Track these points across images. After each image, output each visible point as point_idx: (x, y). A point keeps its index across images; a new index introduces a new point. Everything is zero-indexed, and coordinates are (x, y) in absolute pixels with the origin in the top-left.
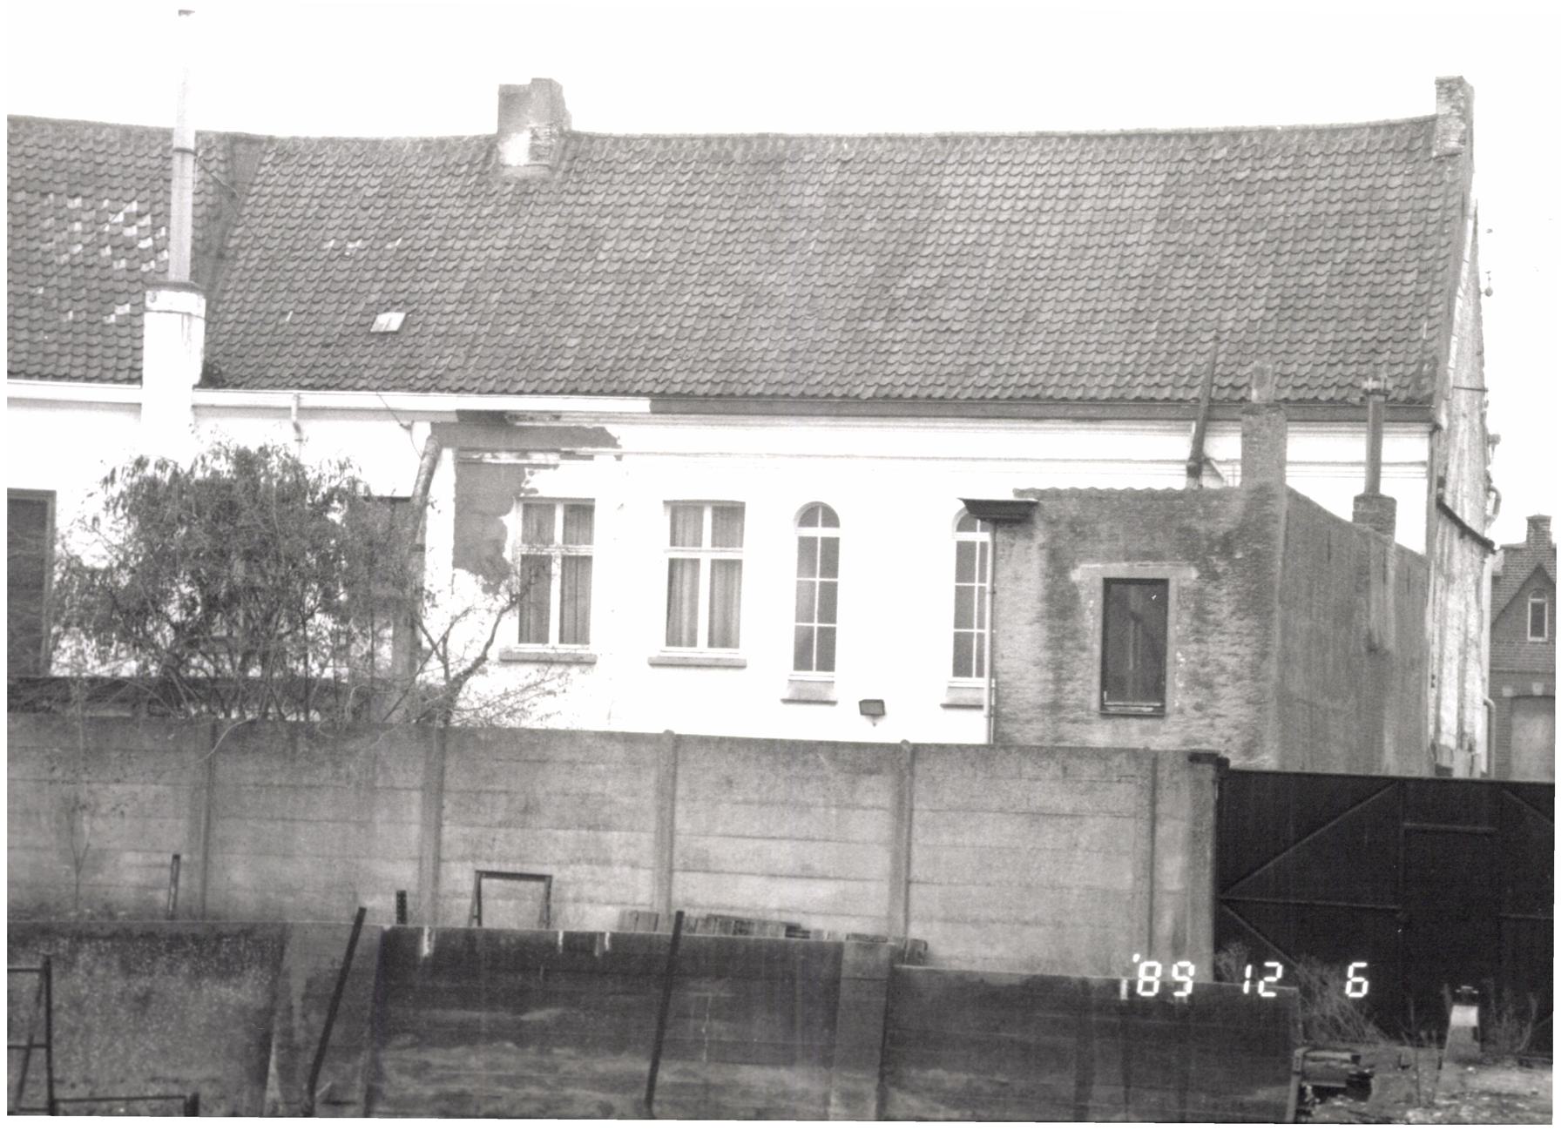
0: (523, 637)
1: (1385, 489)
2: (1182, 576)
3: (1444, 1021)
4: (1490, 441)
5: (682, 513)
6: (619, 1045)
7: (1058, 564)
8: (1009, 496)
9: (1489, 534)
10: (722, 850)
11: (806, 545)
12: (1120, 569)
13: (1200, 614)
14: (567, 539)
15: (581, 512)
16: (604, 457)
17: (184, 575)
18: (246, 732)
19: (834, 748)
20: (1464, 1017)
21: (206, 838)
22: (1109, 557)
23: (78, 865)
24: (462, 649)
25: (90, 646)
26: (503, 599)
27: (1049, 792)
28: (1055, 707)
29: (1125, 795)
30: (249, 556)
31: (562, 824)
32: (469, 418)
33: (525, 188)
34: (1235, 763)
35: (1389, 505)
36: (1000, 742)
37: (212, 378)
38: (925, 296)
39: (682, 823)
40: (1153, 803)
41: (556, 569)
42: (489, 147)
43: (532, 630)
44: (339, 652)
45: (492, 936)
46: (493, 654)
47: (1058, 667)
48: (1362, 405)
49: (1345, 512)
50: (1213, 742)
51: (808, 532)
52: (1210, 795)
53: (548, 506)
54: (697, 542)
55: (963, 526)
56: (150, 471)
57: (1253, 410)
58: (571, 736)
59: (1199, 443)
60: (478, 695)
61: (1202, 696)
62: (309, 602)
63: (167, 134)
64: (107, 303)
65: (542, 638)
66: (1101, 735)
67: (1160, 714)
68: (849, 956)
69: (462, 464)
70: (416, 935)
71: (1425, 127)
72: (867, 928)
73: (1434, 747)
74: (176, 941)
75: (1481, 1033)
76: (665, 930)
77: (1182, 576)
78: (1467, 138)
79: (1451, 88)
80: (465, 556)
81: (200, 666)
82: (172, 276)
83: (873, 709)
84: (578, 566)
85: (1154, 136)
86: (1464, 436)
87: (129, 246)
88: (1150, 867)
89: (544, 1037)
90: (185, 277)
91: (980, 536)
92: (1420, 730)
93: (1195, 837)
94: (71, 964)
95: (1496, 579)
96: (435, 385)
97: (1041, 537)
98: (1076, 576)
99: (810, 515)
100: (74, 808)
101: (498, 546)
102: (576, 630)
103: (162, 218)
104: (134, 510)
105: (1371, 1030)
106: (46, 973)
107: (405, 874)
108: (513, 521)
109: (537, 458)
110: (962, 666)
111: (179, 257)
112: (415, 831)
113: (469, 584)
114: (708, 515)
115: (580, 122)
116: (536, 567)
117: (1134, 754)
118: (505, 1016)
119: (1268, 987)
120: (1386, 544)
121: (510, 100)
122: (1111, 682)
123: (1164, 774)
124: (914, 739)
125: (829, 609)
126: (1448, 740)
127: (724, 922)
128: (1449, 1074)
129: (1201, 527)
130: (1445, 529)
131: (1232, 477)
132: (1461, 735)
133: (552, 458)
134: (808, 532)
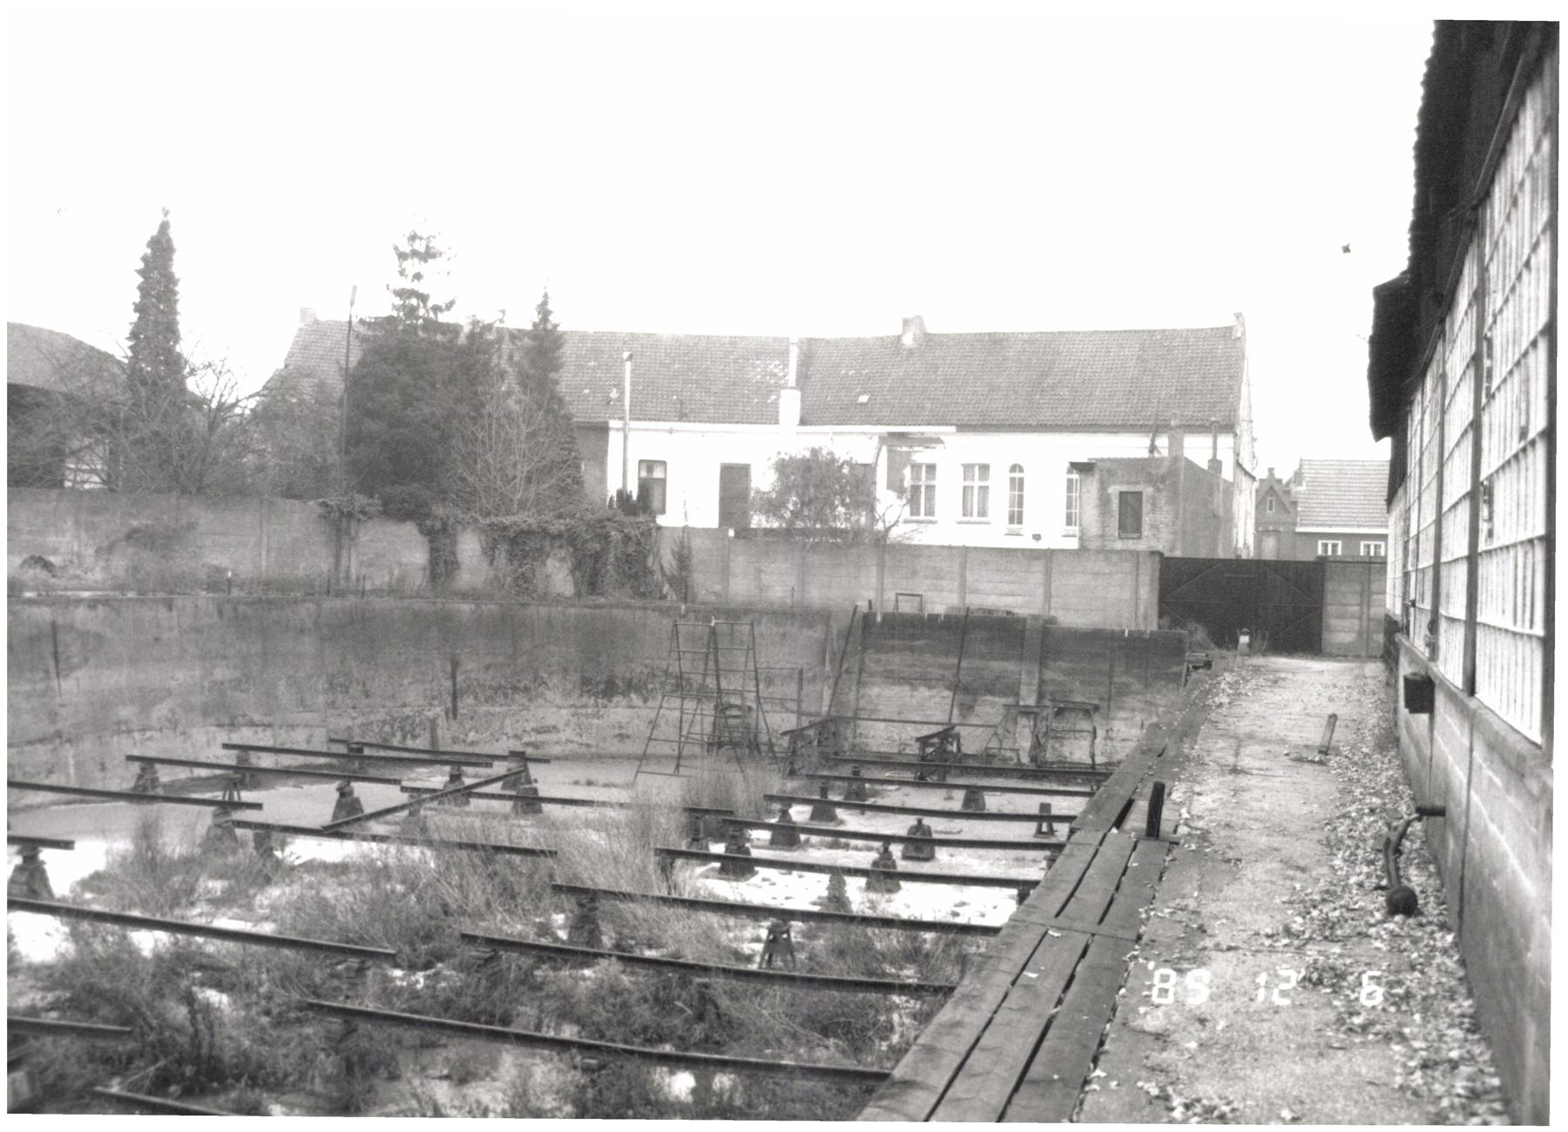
0: (912, 514)
1: (1218, 457)
2: (1148, 491)
3: (1237, 641)
4: (1254, 440)
5: (968, 468)
6: (947, 653)
7: (1103, 487)
8: (1086, 461)
9: (1254, 474)
10: (983, 586)
11: (1012, 480)
12: (1125, 488)
13: (1154, 504)
14: (927, 478)
15: (931, 468)
16: (939, 447)
17: (794, 493)
18: (814, 547)
19: (1023, 551)
20: (1244, 639)
21: (802, 582)
22: (1122, 483)
23: (761, 590)
24: (890, 520)
25: (763, 518)
26: (904, 501)
27: (1100, 565)
28: (1102, 536)
29: (1127, 566)
30: (816, 486)
31: (927, 577)
32: (891, 435)
33: (911, 352)
34: (1167, 554)
35: (1220, 463)
36: (1083, 548)
37: (803, 422)
38: (1054, 387)
39: (969, 578)
40: (1138, 569)
41: (923, 490)
42: (899, 338)
43: (915, 511)
44: (847, 520)
45: (901, 615)
46: (901, 520)
47: (1103, 522)
48: (1210, 427)
49: (1204, 465)
50: (1160, 547)
51: (1013, 475)
52: (1158, 566)
53: (920, 466)
54: (973, 479)
55: (1069, 472)
56: (782, 456)
57: (1172, 429)
58: (929, 547)
59: (1153, 441)
60: (895, 534)
61: (1154, 531)
62: (837, 502)
63: (788, 339)
64: (768, 396)
65: (918, 513)
66: (1119, 545)
67: (1140, 538)
68: (1029, 621)
69: (889, 451)
70: (875, 615)
71: (1230, 329)
72: (1035, 612)
73: (1236, 548)
74: (793, 615)
75: (1250, 645)
76: (963, 613)
77: (1148, 491)
78: (1244, 333)
79: (1238, 316)
80: (890, 486)
81: (799, 524)
82: (790, 385)
83: (1037, 537)
84: (931, 488)
85: (1135, 331)
86: (1245, 439)
87: (775, 375)
88: (1136, 591)
89: (922, 651)
90: (794, 385)
91: (1075, 476)
92: (1231, 541)
93: (1152, 580)
94: (760, 623)
95: (1257, 491)
96: (879, 423)
97: (1097, 476)
98: (1110, 490)
99: (1014, 468)
100: (759, 571)
101: (902, 481)
102: (930, 511)
103: (786, 365)
104: (777, 470)
105: (1212, 645)
106: (752, 625)
107: (871, 595)
108: (907, 472)
109: (916, 449)
110: (1069, 522)
111: (792, 378)
112: (874, 580)
113: (892, 495)
114: (977, 469)
115: (931, 329)
116: (915, 489)
117: (1131, 552)
118: (908, 643)
119: (1284, 994)
120: (1219, 478)
121: (906, 322)
122: (1122, 527)
123: (1141, 560)
124: (1052, 547)
125: (1021, 504)
126: (1241, 545)
127: (984, 610)
128: (1239, 659)
129: (1154, 472)
130: (1239, 471)
131: (1165, 453)
132: (1245, 544)
133: (921, 448)
134: (1013, 475)
